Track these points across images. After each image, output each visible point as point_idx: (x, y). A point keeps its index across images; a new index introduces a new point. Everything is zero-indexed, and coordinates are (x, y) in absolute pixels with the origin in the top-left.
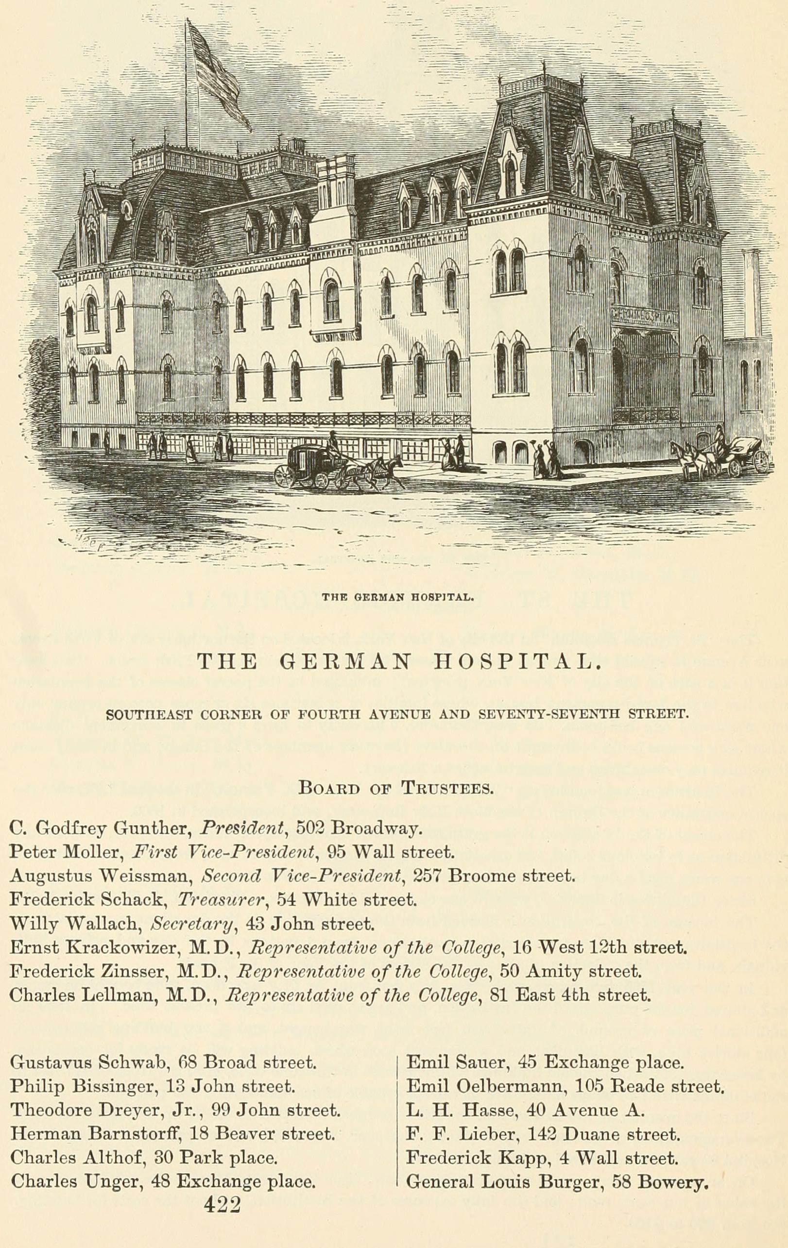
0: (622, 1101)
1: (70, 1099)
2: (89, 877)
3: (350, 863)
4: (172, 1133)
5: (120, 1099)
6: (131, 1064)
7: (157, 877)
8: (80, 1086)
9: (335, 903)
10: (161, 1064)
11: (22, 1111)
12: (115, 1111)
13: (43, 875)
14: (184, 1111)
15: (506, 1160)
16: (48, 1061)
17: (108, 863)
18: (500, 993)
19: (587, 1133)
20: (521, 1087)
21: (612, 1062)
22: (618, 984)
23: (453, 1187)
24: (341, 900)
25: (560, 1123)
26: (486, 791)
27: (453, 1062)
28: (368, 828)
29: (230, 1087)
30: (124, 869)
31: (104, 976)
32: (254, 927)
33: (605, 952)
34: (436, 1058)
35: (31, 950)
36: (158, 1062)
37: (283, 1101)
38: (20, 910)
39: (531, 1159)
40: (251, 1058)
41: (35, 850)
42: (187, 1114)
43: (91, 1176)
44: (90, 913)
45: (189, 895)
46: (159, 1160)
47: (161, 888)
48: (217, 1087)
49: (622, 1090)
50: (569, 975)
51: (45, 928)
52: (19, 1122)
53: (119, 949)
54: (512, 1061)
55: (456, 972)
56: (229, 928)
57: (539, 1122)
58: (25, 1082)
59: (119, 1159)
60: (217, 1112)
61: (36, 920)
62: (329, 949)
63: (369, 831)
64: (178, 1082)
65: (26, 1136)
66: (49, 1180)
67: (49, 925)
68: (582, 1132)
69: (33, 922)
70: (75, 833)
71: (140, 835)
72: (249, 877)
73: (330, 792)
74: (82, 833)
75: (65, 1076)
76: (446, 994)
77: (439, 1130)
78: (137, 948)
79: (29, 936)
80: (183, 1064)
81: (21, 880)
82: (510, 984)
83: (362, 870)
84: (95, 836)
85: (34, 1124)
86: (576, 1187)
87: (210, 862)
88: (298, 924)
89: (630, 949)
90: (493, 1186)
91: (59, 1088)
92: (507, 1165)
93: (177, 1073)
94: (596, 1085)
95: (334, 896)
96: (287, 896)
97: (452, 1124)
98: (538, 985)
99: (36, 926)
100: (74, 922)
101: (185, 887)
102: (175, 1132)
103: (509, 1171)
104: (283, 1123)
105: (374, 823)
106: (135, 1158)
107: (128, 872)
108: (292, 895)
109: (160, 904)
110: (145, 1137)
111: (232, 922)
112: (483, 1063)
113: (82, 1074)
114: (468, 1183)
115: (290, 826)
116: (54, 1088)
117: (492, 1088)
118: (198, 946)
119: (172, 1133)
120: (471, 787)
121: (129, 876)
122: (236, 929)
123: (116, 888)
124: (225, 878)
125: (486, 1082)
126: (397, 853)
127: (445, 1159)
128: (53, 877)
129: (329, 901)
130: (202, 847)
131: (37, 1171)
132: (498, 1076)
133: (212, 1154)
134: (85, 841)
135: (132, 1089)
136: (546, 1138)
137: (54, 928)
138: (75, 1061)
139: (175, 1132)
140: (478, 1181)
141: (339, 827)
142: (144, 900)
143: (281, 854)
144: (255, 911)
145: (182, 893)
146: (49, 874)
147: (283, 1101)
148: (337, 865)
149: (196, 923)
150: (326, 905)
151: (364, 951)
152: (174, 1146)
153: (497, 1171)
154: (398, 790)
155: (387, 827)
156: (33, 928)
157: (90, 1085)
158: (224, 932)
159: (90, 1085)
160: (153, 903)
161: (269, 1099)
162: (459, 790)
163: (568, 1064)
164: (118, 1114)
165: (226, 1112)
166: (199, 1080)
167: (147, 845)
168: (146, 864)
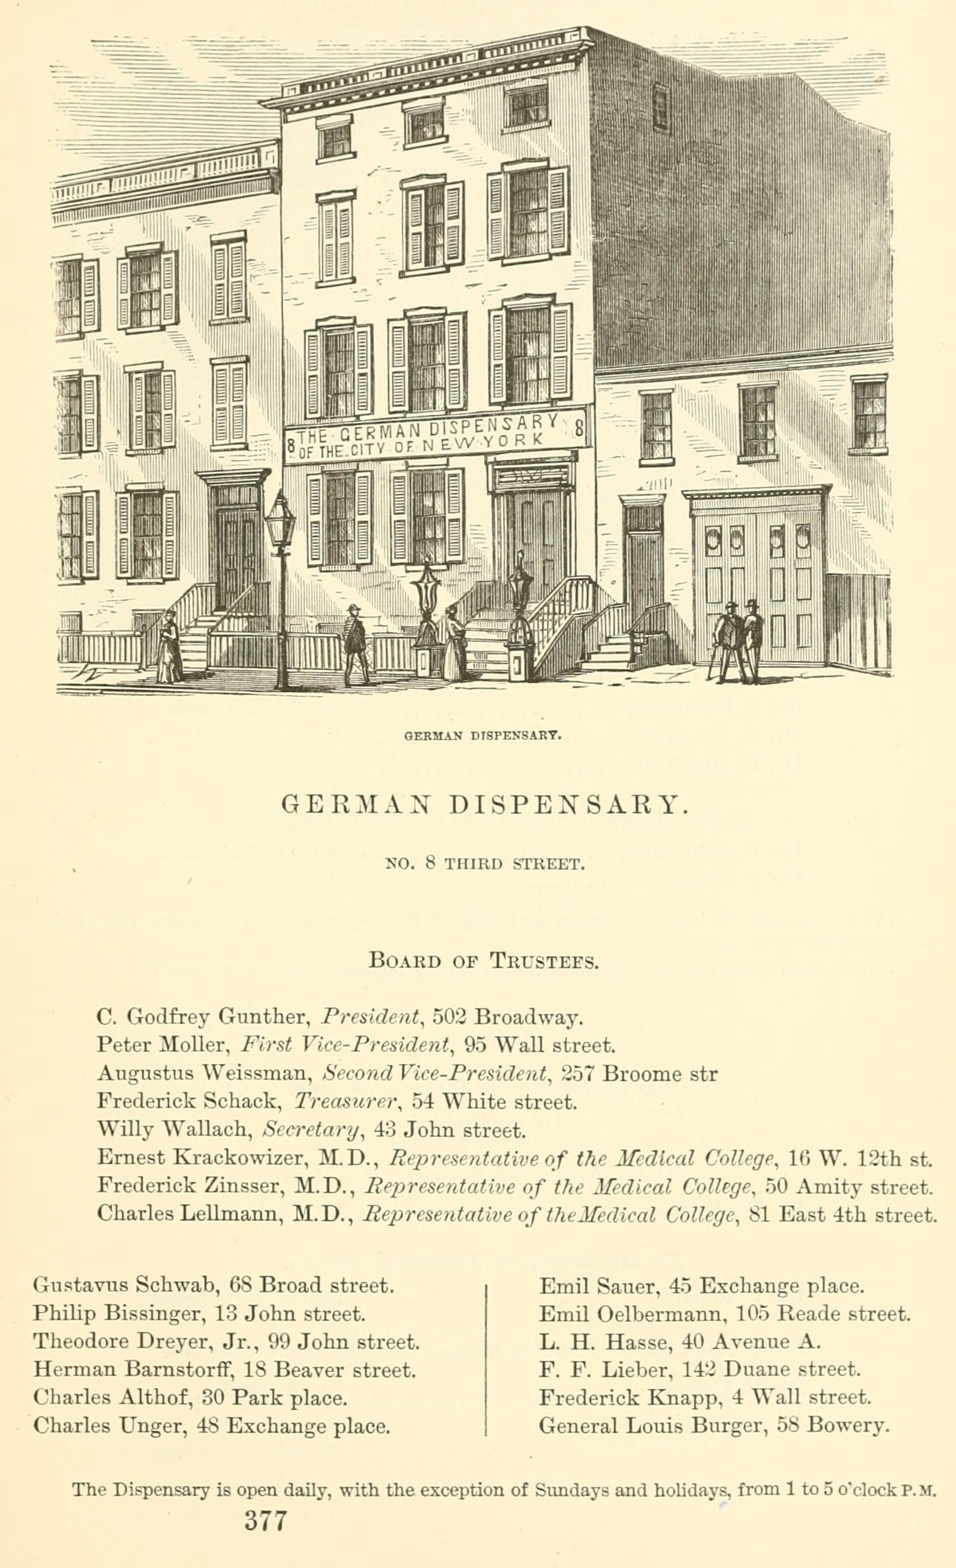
0: (795, 1330)
1: (104, 1328)
2: (190, 1075)
3: (492, 1058)
4: (223, 1370)
5: (160, 1329)
6: (174, 1287)
7: (273, 1075)
8: (112, 1312)
9: (480, 1105)
10: (209, 1286)
11: (47, 1343)
12: (156, 1342)
13: (136, 1072)
14: (236, 1343)
15: (656, 1401)
16: (77, 1282)
17: (212, 1057)
18: (761, 1212)
19: (752, 1367)
20: (673, 1316)
21: (779, 1286)
22: (898, 1203)
23: (594, 1432)
24: (487, 1103)
25: (721, 1357)
26: (590, 965)
27: (593, 1286)
28: (518, 1016)
29: (290, 1315)
30: (231, 1065)
31: (207, 1191)
32: (384, 1134)
33: (875, 1165)
34: (574, 1282)
35: (122, 1160)
36: (206, 1285)
37: (351, 1331)
38: (109, 1113)
39: (699, 1399)
40: (316, 1280)
41: (126, 1042)
42: (240, 1347)
43: (126, 1420)
44: (191, 1117)
45: (307, 1095)
46: (208, 1401)
47: (275, 1088)
48: (273, 1314)
49: (791, 1318)
50: (846, 1191)
51: (138, 1134)
52: (43, 1356)
53: (235, 1159)
54: (663, 1285)
55: (714, 1187)
56: (354, 1135)
57: (695, 1356)
58: (50, 1308)
59: (161, 1399)
60: (274, 1345)
61: (127, 1125)
62: (481, 1160)
63: (519, 1020)
64: (228, 1308)
65: (51, 1372)
66: (77, 1424)
67: (142, 1131)
68: (746, 1367)
69: (124, 1127)
70: (173, 1022)
71: (250, 1025)
72: (379, 1075)
73: (405, 965)
74: (181, 1023)
75: (96, 1301)
76: (698, 1214)
77: (547, 1365)
78: (258, 1159)
79: (119, 1144)
80: (235, 1287)
81: (110, 1079)
82: (774, 1202)
83: (500, 1067)
84: (196, 1025)
85: (60, 1358)
86: (734, 1432)
87: (330, 1057)
88: (436, 1130)
89: (906, 1161)
90: (639, 1431)
91: (89, 1316)
92: (657, 1407)
93: (228, 1297)
94: (760, 1312)
95: (479, 1097)
96: (424, 1097)
97: (594, 1359)
98: (809, 1203)
99: (128, 1132)
100: (172, 1127)
101: (303, 1086)
102: (226, 1367)
103: (659, 1414)
104: (355, 1358)
105: (524, 1012)
106: (180, 1398)
107: (236, 1068)
108: (430, 1096)
109: (273, 1107)
110: (191, 1374)
111: (357, 1128)
112: (628, 1288)
113: (117, 1298)
114: (611, 1427)
115: (427, 1015)
116: (83, 1315)
117: (639, 1316)
118: (328, 1156)
119: (223, 1370)
120: (572, 960)
121: (237, 1073)
122: (363, 1136)
123: (221, 1087)
124: (351, 1075)
125: (632, 1309)
126: (548, 1046)
127: (585, 1399)
128: (147, 1074)
129: (473, 1104)
130: (318, 1039)
131: (66, 1414)
132: (645, 1302)
133: (270, 1393)
134: (185, 1032)
135: (174, 1317)
136: (703, 1374)
137: (148, 1134)
138: (109, 1283)
139: (226, 1367)
140: (623, 1425)
141: (484, 1016)
142: (255, 1101)
143: (410, 1047)
144: (386, 1114)
145: (299, 1093)
146: (143, 1071)
147: (351, 1331)
148: (475, 1060)
149: (316, 1128)
150: (470, 1107)
151: (523, 1163)
152: (227, 1385)
153: (645, 1413)
154: (485, 963)
155: (540, 1015)
156: (124, 1134)
157: (125, 1311)
158: (348, 1139)
159: (125, 1311)
160: (264, 1105)
161: (337, 1329)
162: (557, 964)
163: (727, 1288)
164: (159, 1347)
165: (285, 1345)
166: (253, 1307)
167: (258, 1037)
168: (256, 1059)
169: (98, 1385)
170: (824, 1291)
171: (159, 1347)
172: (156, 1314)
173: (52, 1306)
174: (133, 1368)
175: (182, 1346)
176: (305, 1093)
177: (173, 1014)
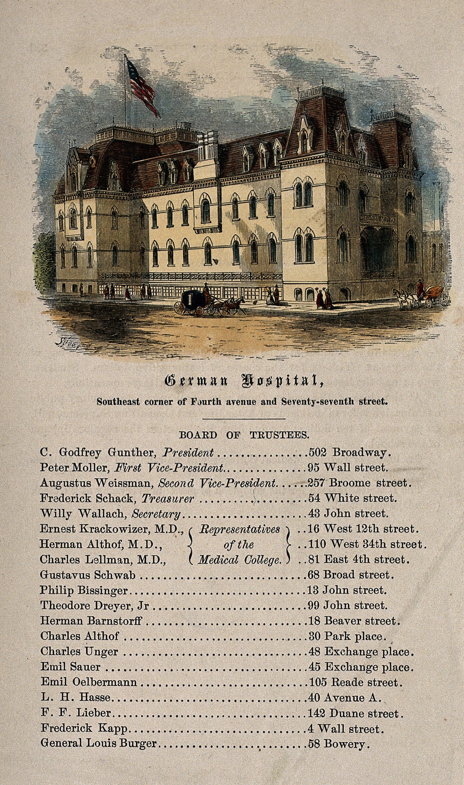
1: (77, 598)
4: (137, 621)
5: (105, 599)
6: (114, 576)
8: (82, 590)
14: (144, 606)
17: (100, 475)
35: (53, 530)
38: (47, 505)
45: (148, 495)
51: (64, 516)
58: (48, 588)
59: (105, 637)
67: (66, 514)
69: (56, 513)
79: (52, 521)
91: (70, 592)
99: (58, 515)
102: (139, 620)
113: (84, 582)
119: (137, 621)
121: (114, 483)
123: (105, 491)
134: (85, 461)
135: (114, 592)
138: (80, 574)
139: (139, 620)
159: (88, 589)
164: (105, 609)
168: (123, 476)
169: (73, 629)
170: (391, 654)
171: (105, 609)
172: (103, 591)
173: (50, 586)
174: (92, 620)
175: (117, 608)
176: (147, 495)
177: (82, 451)
